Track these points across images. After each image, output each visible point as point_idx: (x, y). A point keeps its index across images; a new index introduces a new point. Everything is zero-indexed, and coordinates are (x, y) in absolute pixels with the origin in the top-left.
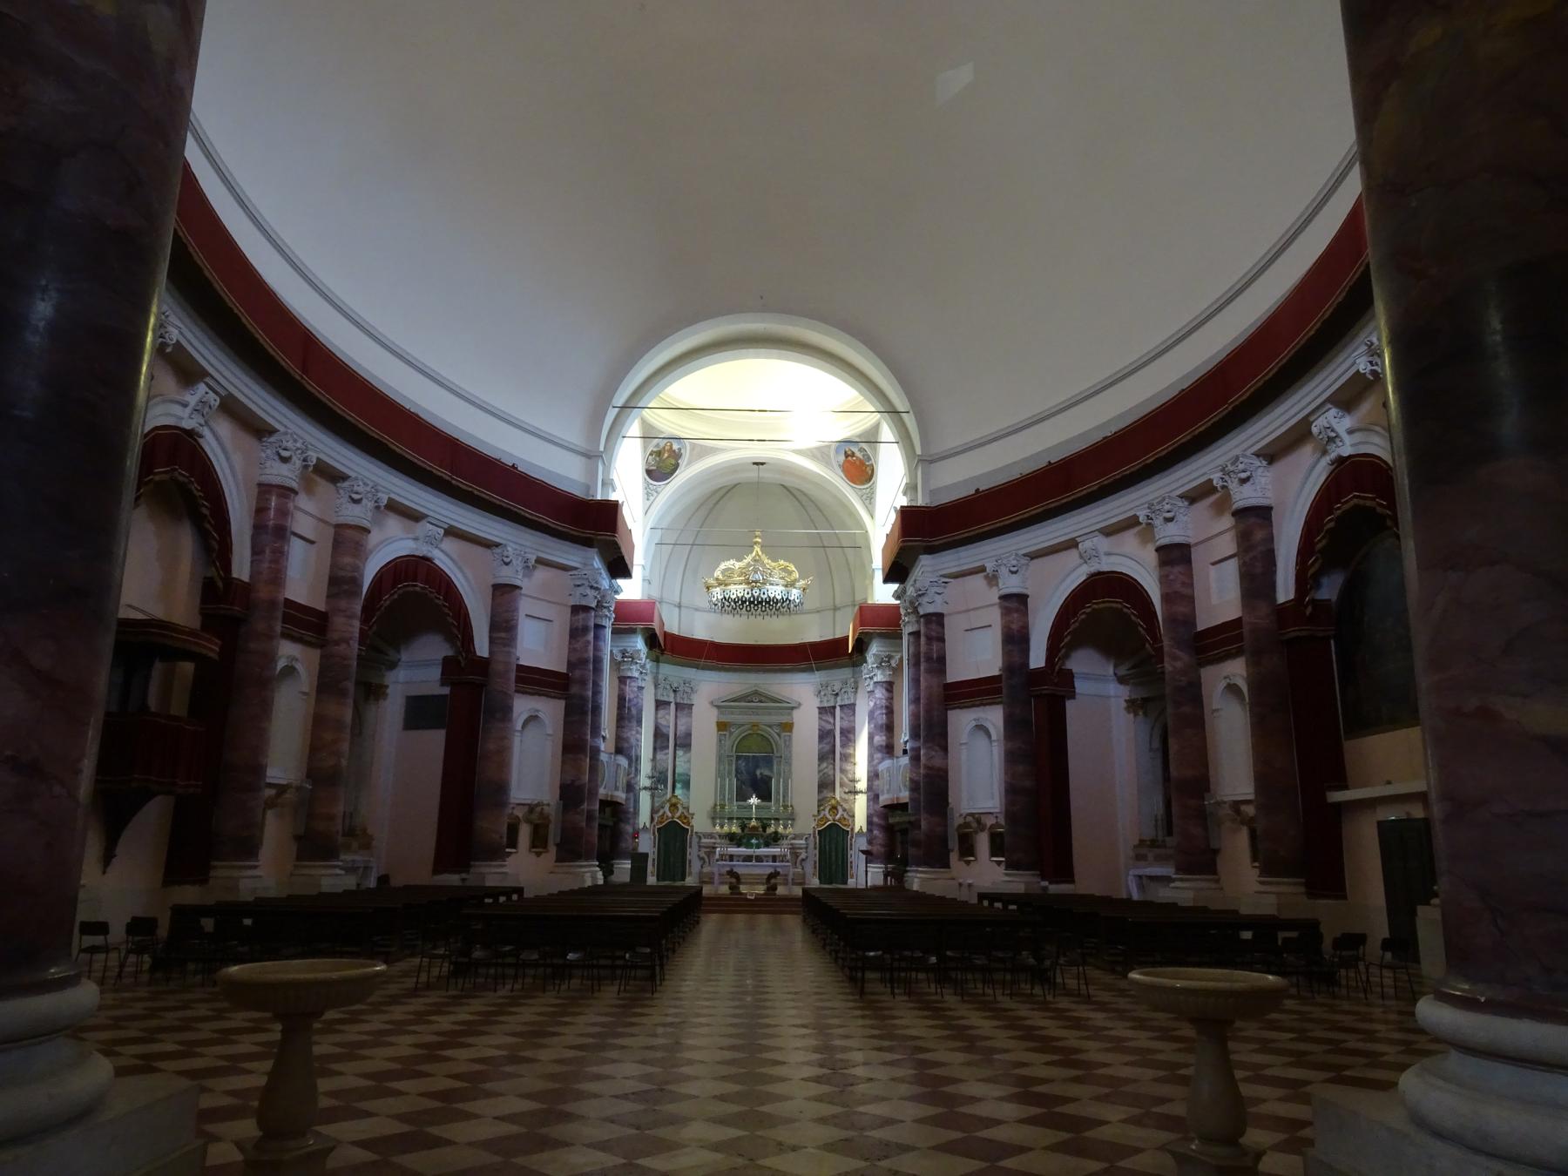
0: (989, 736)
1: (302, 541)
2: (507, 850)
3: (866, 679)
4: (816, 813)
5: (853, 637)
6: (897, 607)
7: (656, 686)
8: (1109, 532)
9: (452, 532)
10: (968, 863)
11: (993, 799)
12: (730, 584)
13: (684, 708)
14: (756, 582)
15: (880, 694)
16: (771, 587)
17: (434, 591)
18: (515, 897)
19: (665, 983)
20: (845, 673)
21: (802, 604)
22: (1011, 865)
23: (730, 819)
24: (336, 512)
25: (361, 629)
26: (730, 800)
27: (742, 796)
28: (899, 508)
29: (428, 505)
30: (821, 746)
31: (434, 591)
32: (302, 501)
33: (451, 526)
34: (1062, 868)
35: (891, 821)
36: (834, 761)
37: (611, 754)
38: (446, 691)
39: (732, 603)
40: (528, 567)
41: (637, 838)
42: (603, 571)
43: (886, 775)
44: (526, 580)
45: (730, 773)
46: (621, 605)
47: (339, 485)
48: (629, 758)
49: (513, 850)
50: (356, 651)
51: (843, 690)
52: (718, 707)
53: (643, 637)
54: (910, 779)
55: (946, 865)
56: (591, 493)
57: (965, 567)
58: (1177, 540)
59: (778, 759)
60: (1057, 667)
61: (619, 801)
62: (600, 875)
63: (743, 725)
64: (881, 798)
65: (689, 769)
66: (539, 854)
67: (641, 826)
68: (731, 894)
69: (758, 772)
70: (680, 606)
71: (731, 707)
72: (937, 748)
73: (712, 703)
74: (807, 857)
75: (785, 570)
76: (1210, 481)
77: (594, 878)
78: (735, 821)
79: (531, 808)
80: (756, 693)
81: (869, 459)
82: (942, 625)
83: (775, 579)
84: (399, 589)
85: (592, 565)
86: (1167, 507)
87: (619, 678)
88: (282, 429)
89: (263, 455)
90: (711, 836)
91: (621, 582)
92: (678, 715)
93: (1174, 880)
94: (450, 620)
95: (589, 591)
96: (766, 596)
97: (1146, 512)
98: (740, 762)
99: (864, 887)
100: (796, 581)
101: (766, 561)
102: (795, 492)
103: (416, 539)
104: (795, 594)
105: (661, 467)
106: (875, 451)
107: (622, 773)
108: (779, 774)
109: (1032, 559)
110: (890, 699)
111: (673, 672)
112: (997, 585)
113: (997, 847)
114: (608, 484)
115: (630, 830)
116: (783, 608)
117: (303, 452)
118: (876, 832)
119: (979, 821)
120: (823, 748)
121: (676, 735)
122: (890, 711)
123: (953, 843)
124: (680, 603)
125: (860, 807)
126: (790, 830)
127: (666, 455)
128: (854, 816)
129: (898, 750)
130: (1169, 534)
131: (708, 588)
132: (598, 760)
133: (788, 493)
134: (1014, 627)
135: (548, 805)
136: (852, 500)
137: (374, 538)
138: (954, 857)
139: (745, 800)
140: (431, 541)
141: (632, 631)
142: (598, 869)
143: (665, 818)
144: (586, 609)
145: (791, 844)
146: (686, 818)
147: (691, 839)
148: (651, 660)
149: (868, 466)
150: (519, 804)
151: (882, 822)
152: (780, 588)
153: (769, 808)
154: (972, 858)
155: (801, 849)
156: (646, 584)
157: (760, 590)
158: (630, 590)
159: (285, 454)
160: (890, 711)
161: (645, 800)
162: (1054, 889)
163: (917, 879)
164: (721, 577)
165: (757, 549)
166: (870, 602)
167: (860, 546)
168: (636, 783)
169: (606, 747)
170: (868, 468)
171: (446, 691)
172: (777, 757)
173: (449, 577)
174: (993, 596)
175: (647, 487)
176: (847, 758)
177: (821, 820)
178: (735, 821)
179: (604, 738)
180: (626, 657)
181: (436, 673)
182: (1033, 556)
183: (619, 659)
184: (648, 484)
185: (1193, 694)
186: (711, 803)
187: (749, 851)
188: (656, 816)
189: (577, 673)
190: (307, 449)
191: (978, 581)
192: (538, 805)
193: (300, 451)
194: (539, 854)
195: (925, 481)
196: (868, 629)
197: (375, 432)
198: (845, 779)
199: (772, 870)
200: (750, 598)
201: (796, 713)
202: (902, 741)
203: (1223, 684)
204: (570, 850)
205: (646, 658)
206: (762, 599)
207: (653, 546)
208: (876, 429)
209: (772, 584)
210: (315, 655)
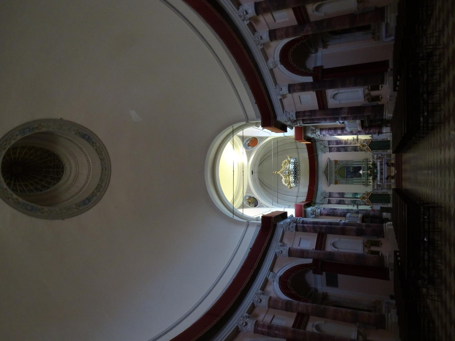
0: (337, 94)
1: (274, 319)
2: (380, 255)
3: (319, 137)
4: (365, 152)
5: (306, 142)
6: (296, 128)
7: (323, 204)
8: (267, 59)
9: (272, 269)
10: (382, 98)
11: (358, 91)
12: (290, 181)
13: (330, 195)
14: (289, 173)
15: (324, 132)
16: (290, 168)
17: (290, 276)
18: (398, 254)
19: (436, 202)
20: (318, 144)
21: (296, 158)
22: (382, 82)
23: (368, 179)
24: (264, 307)
25: (303, 302)
26: (361, 180)
27: (360, 176)
28: (262, 128)
29: (262, 277)
30: (342, 151)
31: (290, 276)
32: (261, 318)
33: (269, 270)
34: (384, 64)
35: (367, 125)
36: (347, 147)
37: (346, 219)
38: (324, 273)
39: (296, 180)
40: (283, 245)
41: (375, 210)
42: (284, 221)
43: (352, 128)
44: (287, 246)
45: (352, 180)
46: (297, 215)
47: (255, 306)
48: (347, 213)
49: (380, 252)
50: (310, 304)
51: (324, 145)
52: (330, 184)
53: (307, 208)
54: (353, 120)
55: (383, 105)
56: (259, 225)
57: (280, 106)
58: (268, 34)
59: (347, 165)
60: (312, 72)
61: (362, 216)
62: (389, 223)
63: (336, 176)
64: (359, 130)
65: (351, 193)
66: (382, 244)
67: (371, 209)
68: (395, 179)
69: (352, 171)
70: (297, 197)
71: (330, 180)
72: (341, 111)
73: (329, 186)
74: (381, 154)
75: (285, 164)
76: (248, 24)
77: (390, 225)
78: (368, 178)
79: (365, 246)
80: (325, 172)
81: (250, 139)
82: (299, 112)
83: (288, 167)
84: (290, 288)
85: (282, 224)
86: (257, 39)
87: (320, 216)
88: (236, 324)
89: (245, 331)
90: (373, 186)
91: (289, 215)
92: (332, 197)
93: (387, 22)
94: (300, 271)
95: (291, 226)
96: (293, 170)
97: (259, 46)
98: (348, 177)
99: (391, 133)
100: (288, 160)
101: (282, 170)
102: (260, 162)
103: (274, 281)
104: (292, 161)
105: (254, 203)
106: (247, 137)
107: (352, 215)
108: (352, 164)
109: (277, 84)
110: (326, 129)
111: (318, 199)
112: (286, 94)
113: (376, 88)
114: (257, 219)
115: (372, 212)
116: (297, 164)
117: (244, 318)
118: (371, 132)
119: (367, 95)
120: (343, 151)
121: (339, 198)
122: (330, 129)
123: (375, 103)
124: (297, 196)
125: (363, 137)
126: (371, 160)
127: (250, 201)
128: (366, 139)
129: (343, 125)
130: (266, 37)
131: (291, 188)
132: (348, 223)
133: (262, 163)
134: (299, 88)
135: (364, 240)
136: (264, 143)
137: (273, 295)
138: (380, 103)
139: (361, 175)
140: (274, 276)
141: (305, 211)
142: (386, 224)
143: (367, 201)
144: (296, 227)
145: (376, 159)
146: (367, 194)
147: (375, 192)
148: (315, 205)
149: (252, 139)
150: (364, 250)
151: (368, 130)
152: (291, 165)
153: (363, 167)
154: (380, 97)
155: (377, 156)
156: (290, 207)
157: (291, 171)
158: (291, 212)
159: (244, 324)
160: (330, 129)
161: (361, 207)
162: (391, 66)
163: (388, 115)
164: (287, 184)
165: (278, 173)
166: (294, 137)
167: (277, 140)
168: (356, 210)
169: (344, 221)
170: (253, 139)
171: (324, 273)
172: (346, 165)
173: (286, 271)
174: (289, 96)
175: (260, 207)
176: (346, 142)
177: (367, 150)
178: (368, 178)
179: (340, 221)
180: (313, 213)
181: (318, 276)
182: (276, 83)
183: (314, 216)
184: (259, 206)
185: (319, 23)
186: (362, 186)
187: (379, 173)
188: (367, 204)
189: (318, 230)
190: (243, 316)
191: (285, 101)
192: (364, 244)
193: (244, 319)
194: (382, 244)
195: (253, 120)
196: (303, 137)
197: (239, 293)
198: (353, 143)
199: (386, 165)
200: (294, 175)
201: (331, 159)
202: (339, 124)
203: (316, 12)
204: (380, 233)
205: (314, 207)
206: (294, 171)
207: (279, 205)
208: (240, 137)
209: (289, 168)
210: (311, 317)
